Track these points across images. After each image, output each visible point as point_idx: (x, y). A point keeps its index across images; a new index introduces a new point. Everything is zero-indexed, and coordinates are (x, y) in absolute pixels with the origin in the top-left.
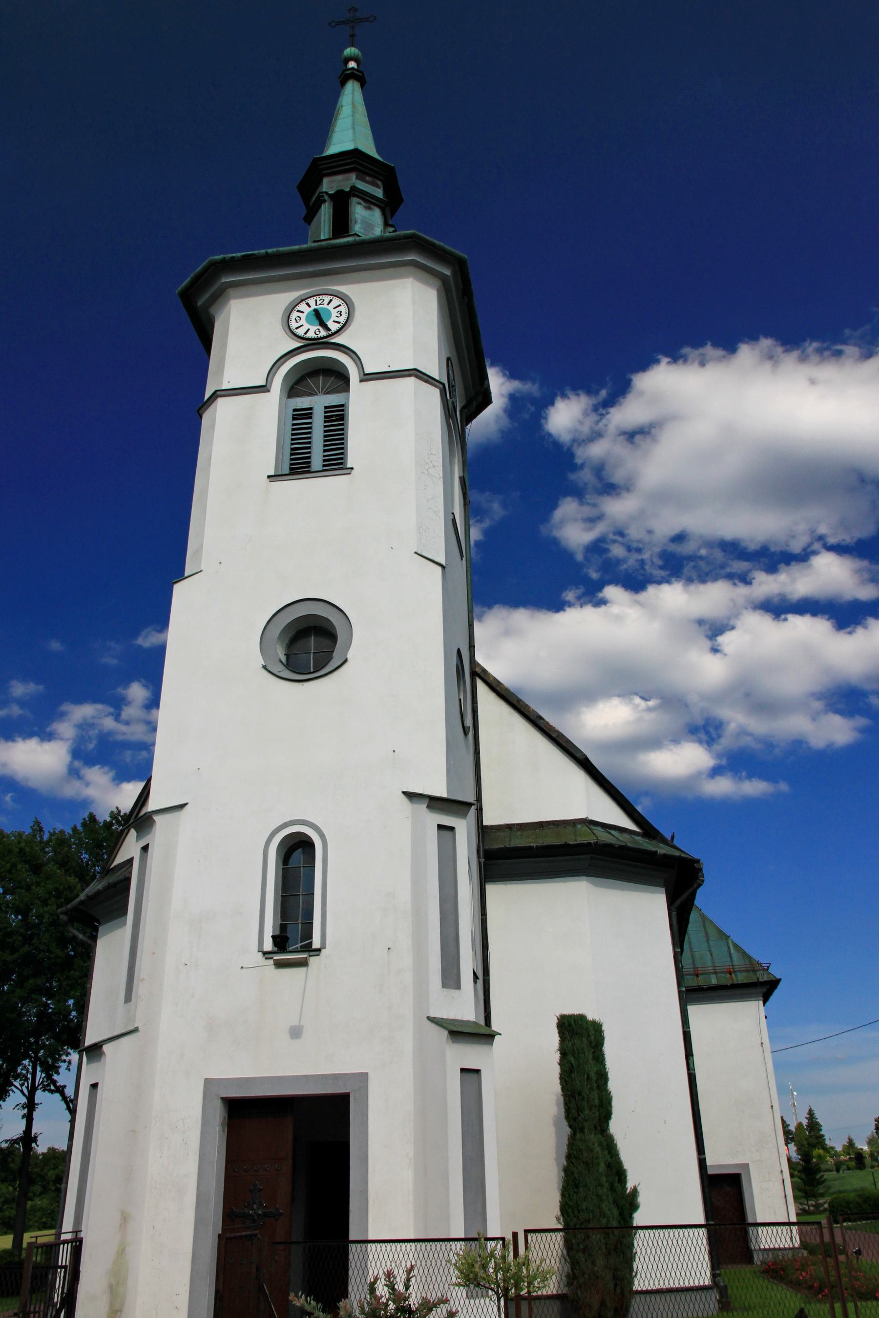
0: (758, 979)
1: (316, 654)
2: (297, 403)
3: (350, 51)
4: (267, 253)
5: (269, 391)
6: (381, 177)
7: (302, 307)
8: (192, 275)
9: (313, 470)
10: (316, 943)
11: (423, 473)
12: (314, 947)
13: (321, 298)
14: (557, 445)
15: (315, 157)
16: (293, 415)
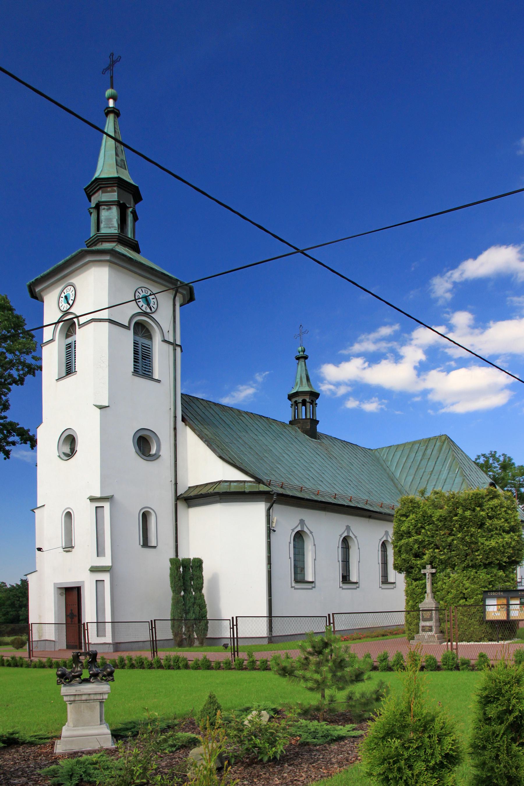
3: (109, 92)
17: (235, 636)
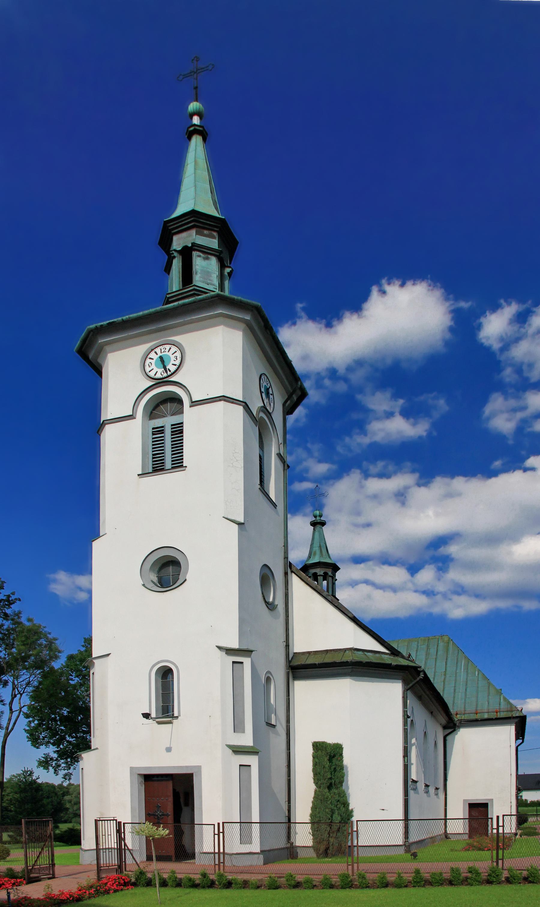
0: (512, 715)
1: (173, 576)
2: (155, 423)
3: (194, 106)
4: (123, 320)
5: (135, 418)
6: (216, 229)
7: (152, 355)
8: (80, 339)
9: (167, 468)
10: (176, 714)
11: (229, 466)
12: (175, 716)
13: (164, 347)
14: (487, 351)
15: (165, 220)
16: (153, 432)
17: (222, 850)
